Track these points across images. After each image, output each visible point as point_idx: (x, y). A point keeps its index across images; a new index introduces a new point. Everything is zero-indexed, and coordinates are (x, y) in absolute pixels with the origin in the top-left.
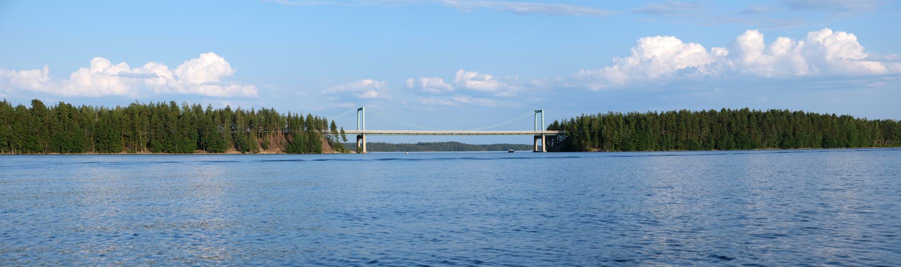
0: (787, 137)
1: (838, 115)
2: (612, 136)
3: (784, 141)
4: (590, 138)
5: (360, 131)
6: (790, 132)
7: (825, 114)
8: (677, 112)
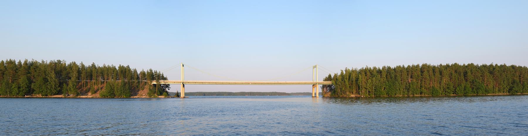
0: (516, 84)
1: (499, 65)
2: (366, 84)
3: (514, 87)
4: (348, 86)
5: (315, 82)
6: (517, 79)
7: (503, 64)
8: (421, 65)
